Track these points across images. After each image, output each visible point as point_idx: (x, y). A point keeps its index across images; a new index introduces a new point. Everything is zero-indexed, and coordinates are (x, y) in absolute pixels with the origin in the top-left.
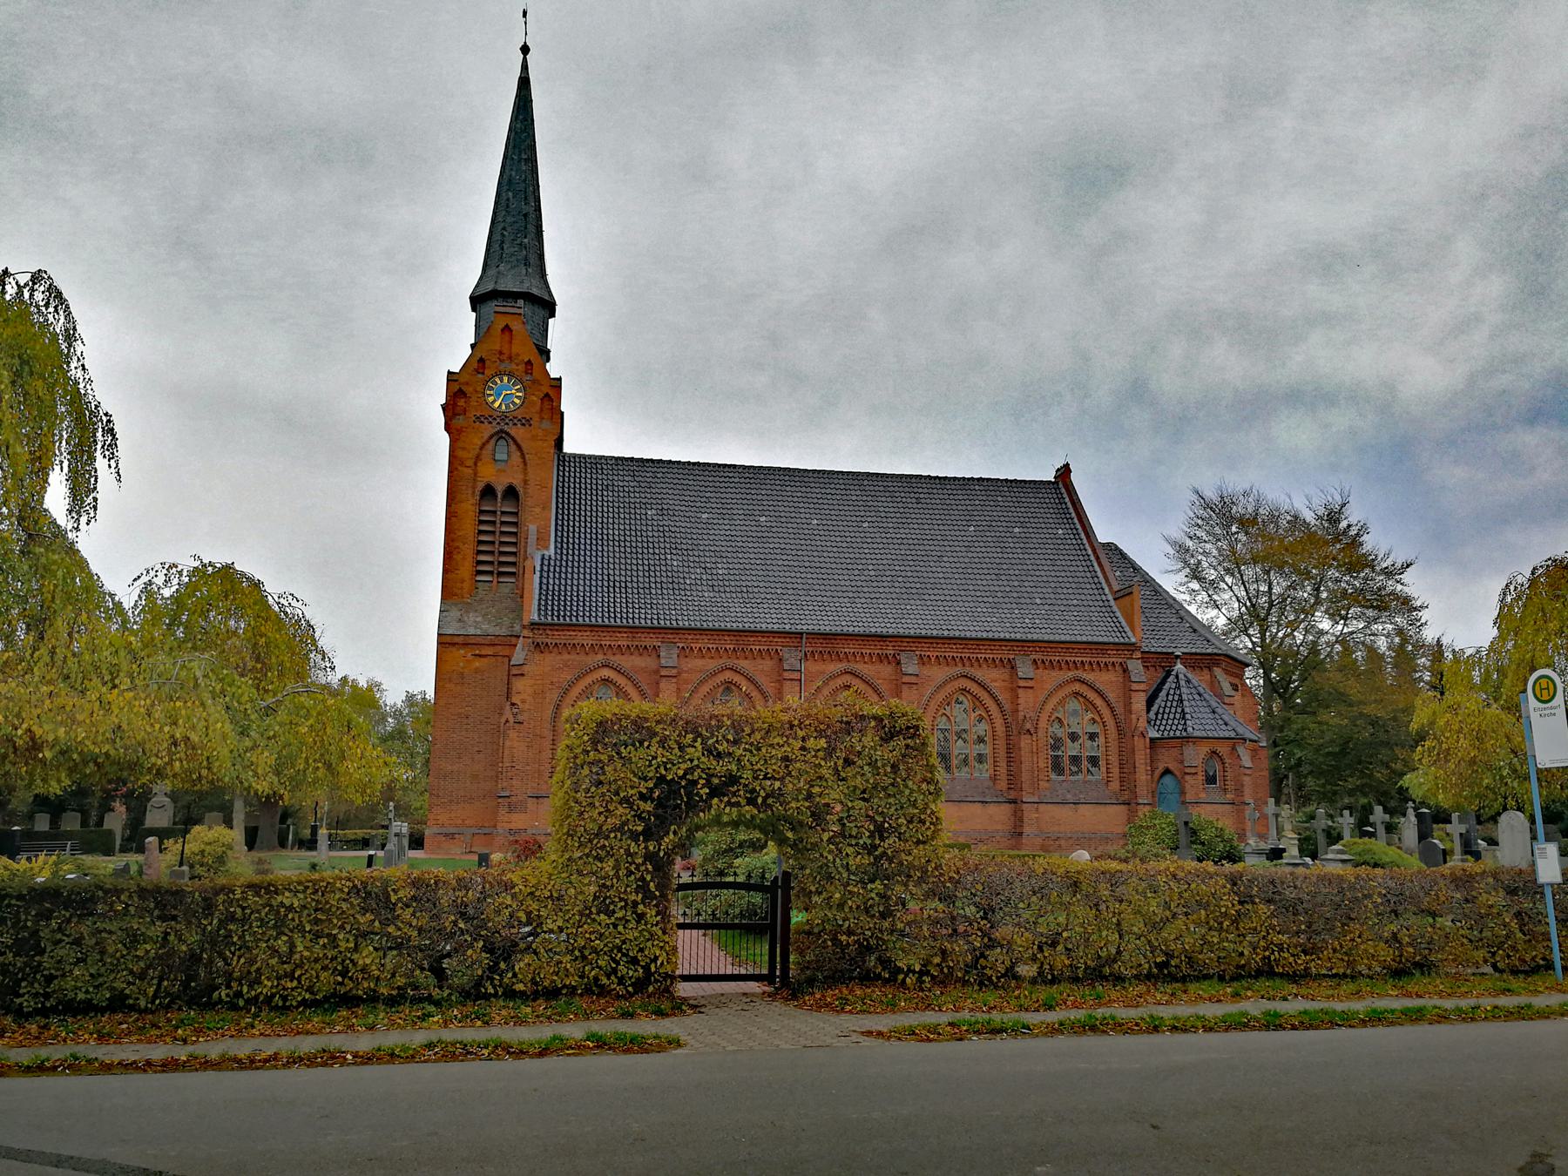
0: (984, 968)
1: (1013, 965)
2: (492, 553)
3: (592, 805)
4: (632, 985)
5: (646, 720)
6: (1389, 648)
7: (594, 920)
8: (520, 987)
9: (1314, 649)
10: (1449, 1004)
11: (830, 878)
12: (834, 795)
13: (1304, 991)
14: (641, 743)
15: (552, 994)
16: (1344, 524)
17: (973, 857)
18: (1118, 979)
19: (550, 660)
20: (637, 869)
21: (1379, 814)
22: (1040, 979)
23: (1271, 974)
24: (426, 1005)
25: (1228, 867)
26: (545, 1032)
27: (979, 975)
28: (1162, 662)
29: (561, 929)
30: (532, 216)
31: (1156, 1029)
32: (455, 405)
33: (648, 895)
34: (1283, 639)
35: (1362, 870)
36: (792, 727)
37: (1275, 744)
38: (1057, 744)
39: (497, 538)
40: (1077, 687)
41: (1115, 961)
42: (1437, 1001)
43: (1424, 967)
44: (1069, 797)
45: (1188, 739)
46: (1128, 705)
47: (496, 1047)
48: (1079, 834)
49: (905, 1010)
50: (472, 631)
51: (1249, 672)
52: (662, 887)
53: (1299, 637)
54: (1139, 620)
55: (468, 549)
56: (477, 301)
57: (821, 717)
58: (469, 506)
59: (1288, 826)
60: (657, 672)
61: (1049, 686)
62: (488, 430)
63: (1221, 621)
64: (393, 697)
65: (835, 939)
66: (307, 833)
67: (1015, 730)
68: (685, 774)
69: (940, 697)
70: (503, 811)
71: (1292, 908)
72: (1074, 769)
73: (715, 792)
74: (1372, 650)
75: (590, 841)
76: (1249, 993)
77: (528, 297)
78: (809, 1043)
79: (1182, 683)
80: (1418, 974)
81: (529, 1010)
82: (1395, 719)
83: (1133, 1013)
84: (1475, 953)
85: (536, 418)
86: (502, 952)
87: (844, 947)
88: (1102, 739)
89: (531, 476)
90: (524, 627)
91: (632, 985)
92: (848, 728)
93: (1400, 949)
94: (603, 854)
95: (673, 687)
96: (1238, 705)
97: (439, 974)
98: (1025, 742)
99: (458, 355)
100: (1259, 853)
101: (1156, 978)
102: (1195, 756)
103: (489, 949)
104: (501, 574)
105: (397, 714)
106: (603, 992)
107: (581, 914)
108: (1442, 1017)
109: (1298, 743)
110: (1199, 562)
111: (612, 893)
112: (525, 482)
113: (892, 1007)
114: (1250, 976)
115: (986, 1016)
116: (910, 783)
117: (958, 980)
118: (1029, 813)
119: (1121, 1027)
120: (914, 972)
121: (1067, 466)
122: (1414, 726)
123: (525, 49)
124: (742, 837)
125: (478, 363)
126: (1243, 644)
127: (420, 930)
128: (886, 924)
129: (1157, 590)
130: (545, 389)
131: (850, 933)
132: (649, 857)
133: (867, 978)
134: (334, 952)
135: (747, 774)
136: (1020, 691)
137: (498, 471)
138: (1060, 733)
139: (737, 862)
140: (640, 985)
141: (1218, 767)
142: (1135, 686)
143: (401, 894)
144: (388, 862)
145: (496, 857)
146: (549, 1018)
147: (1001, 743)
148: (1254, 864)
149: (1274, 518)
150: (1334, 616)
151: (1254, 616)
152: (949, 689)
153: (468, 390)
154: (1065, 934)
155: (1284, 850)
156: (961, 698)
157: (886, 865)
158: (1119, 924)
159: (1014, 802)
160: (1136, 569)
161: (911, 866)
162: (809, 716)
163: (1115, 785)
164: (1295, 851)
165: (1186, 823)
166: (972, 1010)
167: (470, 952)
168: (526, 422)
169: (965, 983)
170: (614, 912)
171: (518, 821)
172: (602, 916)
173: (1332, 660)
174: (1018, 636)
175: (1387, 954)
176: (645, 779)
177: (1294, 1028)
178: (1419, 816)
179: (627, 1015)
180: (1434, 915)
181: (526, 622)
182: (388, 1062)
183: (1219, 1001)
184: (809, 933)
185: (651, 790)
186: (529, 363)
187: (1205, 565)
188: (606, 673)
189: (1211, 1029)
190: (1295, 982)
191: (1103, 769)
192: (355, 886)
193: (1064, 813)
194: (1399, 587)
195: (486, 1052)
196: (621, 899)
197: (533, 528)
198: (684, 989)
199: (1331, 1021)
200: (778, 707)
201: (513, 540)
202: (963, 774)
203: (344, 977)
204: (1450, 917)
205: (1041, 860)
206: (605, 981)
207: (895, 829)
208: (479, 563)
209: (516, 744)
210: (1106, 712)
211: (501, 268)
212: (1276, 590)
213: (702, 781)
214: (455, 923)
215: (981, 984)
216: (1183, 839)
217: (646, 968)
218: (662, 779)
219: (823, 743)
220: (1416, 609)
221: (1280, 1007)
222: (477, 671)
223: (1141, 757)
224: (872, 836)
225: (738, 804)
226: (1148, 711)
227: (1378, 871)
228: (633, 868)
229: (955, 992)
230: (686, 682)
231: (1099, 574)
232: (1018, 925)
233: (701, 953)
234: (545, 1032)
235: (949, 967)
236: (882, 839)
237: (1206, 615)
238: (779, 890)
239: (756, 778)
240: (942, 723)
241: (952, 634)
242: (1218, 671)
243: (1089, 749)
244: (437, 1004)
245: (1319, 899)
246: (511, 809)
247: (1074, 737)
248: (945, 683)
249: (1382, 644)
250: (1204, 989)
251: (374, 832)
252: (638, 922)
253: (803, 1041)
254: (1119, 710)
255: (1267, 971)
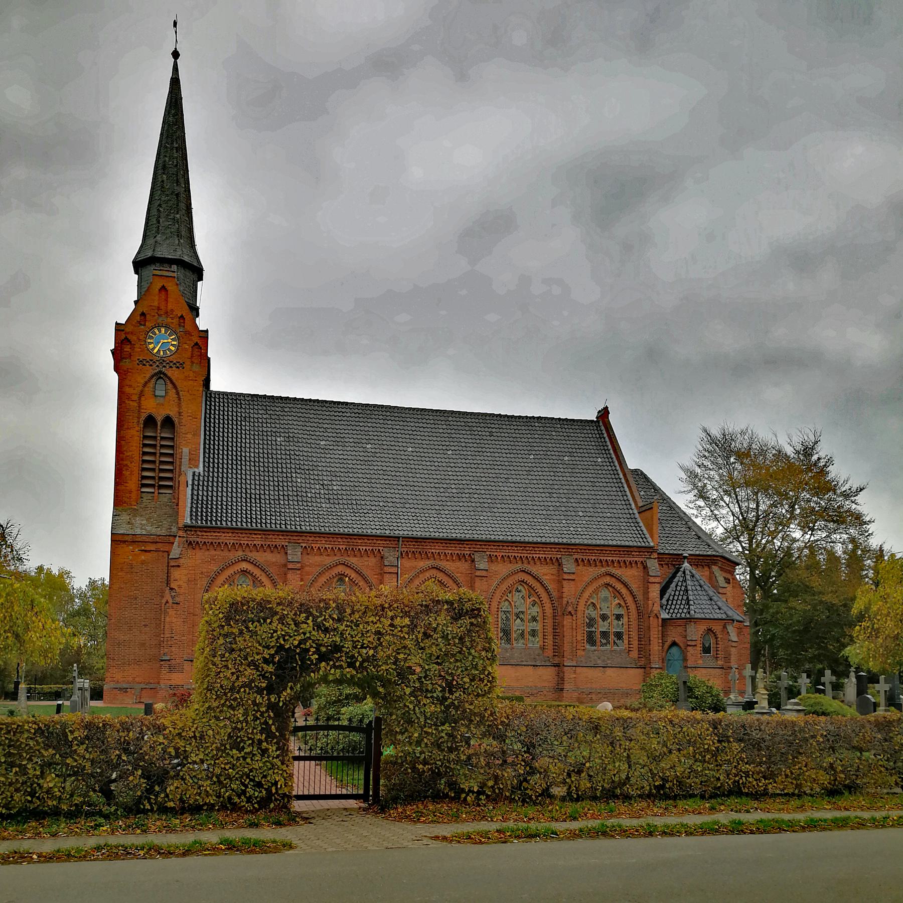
0: (526, 789)
1: (547, 789)
2: (153, 470)
3: (226, 667)
4: (258, 803)
5: (269, 602)
6: (844, 553)
7: (228, 754)
8: (171, 804)
9: (788, 552)
10: (866, 815)
11: (410, 722)
12: (415, 661)
13: (762, 806)
14: (265, 621)
15: (196, 809)
16: (815, 457)
17: (519, 707)
18: (627, 798)
19: (199, 556)
20: (262, 714)
21: (828, 677)
22: (569, 797)
23: (740, 794)
24: (97, 818)
25: (711, 715)
26: (188, 838)
27: (522, 795)
28: (673, 561)
29: (202, 761)
30: (183, 195)
31: (651, 834)
32: (122, 350)
33: (270, 735)
34: (765, 544)
35: (810, 718)
36: (383, 609)
37: (756, 624)
38: (591, 622)
39: (157, 459)
40: (608, 579)
41: (624, 784)
42: (859, 813)
43: (852, 788)
44: (600, 663)
45: (691, 620)
46: (646, 593)
47: (150, 849)
48: (606, 690)
49: (465, 821)
50: (138, 531)
51: (739, 570)
52: (282, 729)
53: (777, 543)
54: (657, 528)
55: (134, 467)
56: (139, 265)
57: (406, 602)
58: (135, 433)
59: (761, 685)
60: (285, 565)
61: (587, 579)
62: (149, 371)
63: (720, 531)
64: (79, 583)
65: (414, 768)
66: (11, 686)
67: (561, 612)
68: (300, 643)
69: (504, 587)
70: (164, 671)
71: (757, 745)
72: (604, 641)
73: (323, 657)
74: (831, 554)
75: (225, 694)
76: (722, 808)
77: (180, 263)
78: (390, 845)
79: (688, 577)
80: (846, 794)
81: (178, 821)
82: (845, 605)
83: (635, 822)
84: (889, 778)
85: (188, 363)
86: (157, 778)
87: (421, 774)
88: (625, 619)
89: (184, 408)
90: (179, 529)
91: (258, 803)
92: (427, 609)
93: (835, 775)
94: (234, 704)
95: (297, 577)
96: (729, 594)
97: (108, 795)
98: (567, 621)
99: (124, 310)
100: (737, 704)
101: (655, 796)
102: (695, 633)
103: (146, 776)
104: (161, 487)
105: (82, 596)
106: (235, 808)
107: (218, 749)
108: (861, 825)
109: (773, 622)
110: (705, 485)
111: (242, 733)
112: (180, 413)
113: (456, 818)
114: (724, 795)
115: (525, 825)
116: (473, 651)
117: (506, 798)
118: (569, 674)
119: (625, 833)
120: (473, 792)
121: (606, 408)
122: (854, 611)
123: (176, 55)
124: (348, 691)
125: (140, 316)
126: (735, 548)
127: (93, 761)
128: (453, 756)
129: (672, 507)
130: (196, 339)
131: (425, 763)
132: (271, 706)
133: (438, 797)
134: (24, 778)
135: (348, 645)
136: (565, 582)
137: (158, 404)
138: (594, 614)
139: (343, 710)
140: (264, 803)
141: (713, 641)
142: (652, 580)
143: (76, 734)
144: (73, 709)
145: (159, 706)
146: (193, 827)
147: (549, 622)
148: (733, 714)
149: (763, 452)
150: (806, 527)
151: (746, 526)
152: (510, 581)
153: (133, 338)
154: (587, 765)
155: (756, 703)
156: (520, 588)
157: (453, 712)
158: (628, 757)
159: (557, 665)
160: (657, 490)
161: (472, 713)
162: (397, 601)
163: (635, 654)
164: (765, 704)
165: (685, 683)
166: (515, 820)
167: (131, 778)
168: (180, 366)
169: (512, 800)
170: (243, 748)
171: (177, 679)
172: (234, 751)
173: (801, 561)
174: (565, 541)
175: (824, 779)
176: (268, 647)
177: (752, 832)
178: (858, 678)
179: (254, 825)
180: (861, 750)
181: (181, 525)
182: (65, 861)
183: (700, 813)
184: (396, 763)
185: (272, 656)
186: (182, 317)
187: (709, 487)
188: (244, 566)
189: (691, 834)
190: (757, 799)
191: (626, 642)
192: (40, 728)
193: (590, 673)
194: (854, 506)
195: (142, 853)
196: (249, 739)
197: (186, 450)
198: (298, 806)
199: (779, 827)
200: (373, 593)
201: (171, 460)
202: (520, 644)
203: (32, 797)
204: (873, 752)
205: (571, 709)
206: (236, 800)
207: (460, 687)
208: (144, 478)
209: (174, 620)
210: (629, 599)
211: (158, 238)
212: (762, 507)
213: (313, 650)
214: (119, 756)
215: (524, 801)
216: (682, 694)
217: (268, 790)
218: (281, 648)
219: (407, 621)
220: (865, 523)
221: (743, 817)
222: (143, 562)
223: (655, 633)
224: (443, 690)
225: (341, 667)
226: (661, 598)
227: (822, 719)
228: (258, 715)
229: (503, 807)
230: (308, 574)
231: (628, 493)
232: (553, 757)
233: (312, 777)
234: (188, 838)
235: (499, 789)
236: (451, 693)
237: (708, 526)
238: (373, 731)
239: (356, 647)
240: (505, 606)
241: (514, 539)
242: (715, 568)
243: (615, 626)
244: (106, 817)
245: (777, 739)
246: (171, 669)
247: (604, 617)
248: (508, 576)
249: (839, 549)
250: (690, 804)
251: (65, 687)
252: (262, 755)
253: (386, 844)
254: (640, 597)
255: (736, 791)
